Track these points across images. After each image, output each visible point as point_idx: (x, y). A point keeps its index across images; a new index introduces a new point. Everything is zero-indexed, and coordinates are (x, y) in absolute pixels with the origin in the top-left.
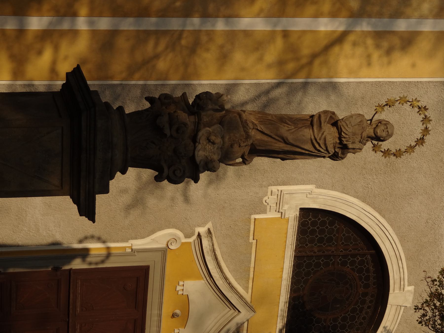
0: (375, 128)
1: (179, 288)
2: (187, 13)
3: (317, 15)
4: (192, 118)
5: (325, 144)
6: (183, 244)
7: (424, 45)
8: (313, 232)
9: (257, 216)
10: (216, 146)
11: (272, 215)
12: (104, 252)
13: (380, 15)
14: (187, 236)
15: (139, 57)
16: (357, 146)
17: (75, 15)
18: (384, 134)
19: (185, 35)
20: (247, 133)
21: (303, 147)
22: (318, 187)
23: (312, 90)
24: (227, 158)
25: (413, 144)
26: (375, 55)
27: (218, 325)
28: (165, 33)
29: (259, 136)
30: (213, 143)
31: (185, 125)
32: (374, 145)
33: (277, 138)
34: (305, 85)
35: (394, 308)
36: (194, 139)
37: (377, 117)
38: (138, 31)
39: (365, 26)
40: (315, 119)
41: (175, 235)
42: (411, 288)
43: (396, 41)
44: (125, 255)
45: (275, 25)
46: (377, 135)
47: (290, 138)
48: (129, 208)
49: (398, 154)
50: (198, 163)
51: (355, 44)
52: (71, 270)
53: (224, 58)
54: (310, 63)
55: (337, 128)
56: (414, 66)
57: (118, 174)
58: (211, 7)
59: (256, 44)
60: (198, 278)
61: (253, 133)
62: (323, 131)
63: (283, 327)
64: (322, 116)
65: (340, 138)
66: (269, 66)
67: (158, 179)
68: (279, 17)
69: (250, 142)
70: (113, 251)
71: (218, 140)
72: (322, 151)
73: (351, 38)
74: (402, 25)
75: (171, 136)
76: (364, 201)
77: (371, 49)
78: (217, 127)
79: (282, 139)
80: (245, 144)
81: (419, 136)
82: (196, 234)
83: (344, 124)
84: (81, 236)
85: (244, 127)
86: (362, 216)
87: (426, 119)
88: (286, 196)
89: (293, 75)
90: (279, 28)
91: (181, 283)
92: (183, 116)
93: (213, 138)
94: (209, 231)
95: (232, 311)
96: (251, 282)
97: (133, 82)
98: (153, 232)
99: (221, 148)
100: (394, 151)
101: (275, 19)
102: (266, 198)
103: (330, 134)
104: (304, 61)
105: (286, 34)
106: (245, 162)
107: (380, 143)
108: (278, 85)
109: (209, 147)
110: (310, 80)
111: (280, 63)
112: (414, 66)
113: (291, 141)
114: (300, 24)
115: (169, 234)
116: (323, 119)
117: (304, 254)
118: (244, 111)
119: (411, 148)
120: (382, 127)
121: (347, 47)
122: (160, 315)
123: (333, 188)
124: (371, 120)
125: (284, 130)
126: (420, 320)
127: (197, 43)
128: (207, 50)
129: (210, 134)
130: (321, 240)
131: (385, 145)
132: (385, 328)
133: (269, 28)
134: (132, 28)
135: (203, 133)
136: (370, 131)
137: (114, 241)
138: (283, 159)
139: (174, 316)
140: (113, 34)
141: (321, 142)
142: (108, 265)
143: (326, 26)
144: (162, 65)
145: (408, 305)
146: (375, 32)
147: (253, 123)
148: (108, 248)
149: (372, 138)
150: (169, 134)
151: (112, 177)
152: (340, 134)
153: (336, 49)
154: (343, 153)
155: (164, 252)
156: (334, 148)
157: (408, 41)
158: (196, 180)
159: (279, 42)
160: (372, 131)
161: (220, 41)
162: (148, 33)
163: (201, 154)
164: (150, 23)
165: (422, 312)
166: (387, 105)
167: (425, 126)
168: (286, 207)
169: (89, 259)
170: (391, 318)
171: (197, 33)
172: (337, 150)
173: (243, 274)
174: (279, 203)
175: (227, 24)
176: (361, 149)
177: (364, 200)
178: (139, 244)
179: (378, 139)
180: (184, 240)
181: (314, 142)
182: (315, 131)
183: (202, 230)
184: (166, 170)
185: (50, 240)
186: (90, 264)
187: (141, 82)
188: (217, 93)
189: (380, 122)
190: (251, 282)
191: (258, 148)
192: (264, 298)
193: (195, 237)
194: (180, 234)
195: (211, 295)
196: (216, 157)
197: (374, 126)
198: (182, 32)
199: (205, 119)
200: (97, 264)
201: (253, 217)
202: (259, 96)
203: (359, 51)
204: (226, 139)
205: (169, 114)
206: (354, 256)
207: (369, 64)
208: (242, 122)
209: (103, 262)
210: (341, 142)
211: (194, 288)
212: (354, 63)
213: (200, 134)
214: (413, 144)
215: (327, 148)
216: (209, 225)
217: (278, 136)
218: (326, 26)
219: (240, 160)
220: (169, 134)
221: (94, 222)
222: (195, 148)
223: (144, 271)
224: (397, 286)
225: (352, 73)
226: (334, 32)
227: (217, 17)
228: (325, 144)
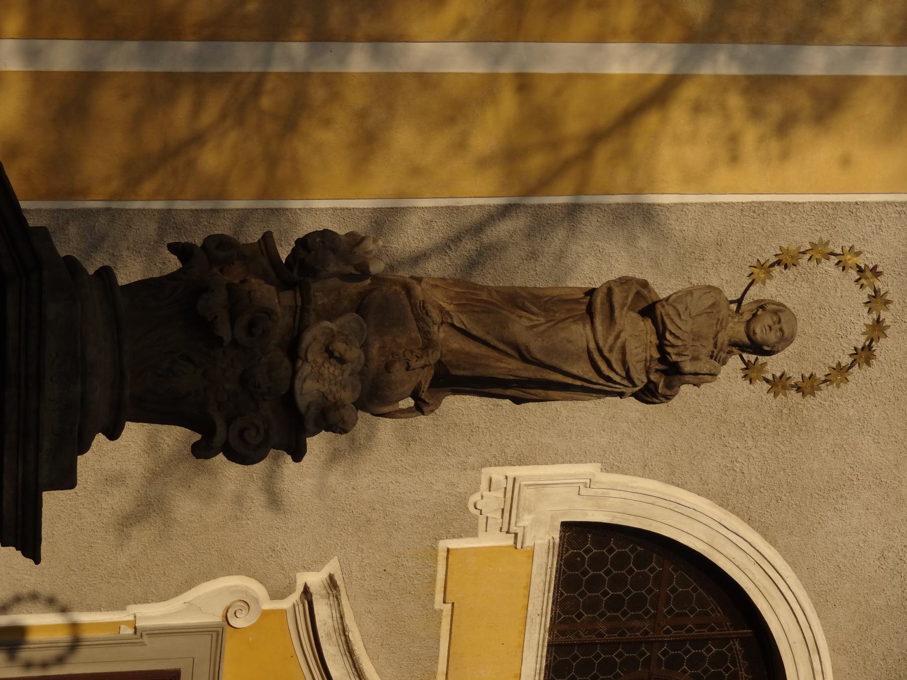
2: (274, 30)
3: (601, 37)
4: (288, 297)
5: (624, 363)
6: (265, 614)
7: (870, 109)
8: (595, 583)
9: (454, 544)
10: (348, 368)
11: (491, 539)
12: (64, 636)
13: (761, 36)
14: (276, 594)
15: (152, 141)
16: (704, 366)
18: (772, 337)
19: (269, 86)
20: (425, 334)
22: (609, 468)
23: (590, 224)
24: (374, 397)
25: (846, 360)
26: (750, 136)
28: (220, 78)
29: (458, 343)
30: (342, 361)
31: (270, 313)
33: (502, 347)
34: (573, 211)
36: (293, 350)
37: (755, 293)
38: (149, 75)
39: (722, 63)
40: (599, 300)
43: (802, 100)
45: (497, 60)
46: (756, 338)
47: (536, 347)
48: (126, 523)
49: (807, 386)
50: (303, 409)
51: (698, 108)
53: (368, 142)
54: (586, 155)
56: (846, 162)
57: (100, 438)
58: (336, 16)
59: (452, 106)
61: (440, 334)
65: (661, 348)
66: (483, 163)
67: (201, 451)
68: (508, 40)
69: (433, 357)
70: (87, 635)
71: (354, 353)
73: (689, 93)
74: (815, 61)
75: (235, 343)
76: (723, 503)
77: (739, 120)
78: (350, 319)
79: (511, 350)
81: (861, 341)
82: (300, 589)
83: (672, 312)
85: (418, 319)
86: (720, 542)
87: (877, 300)
88: (527, 493)
89: (543, 185)
90: (507, 69)
92: (265, 292)
93: (340, 347)
94: (332, 582)
97: (137, 205)
98: (189, 584)
99: (361, 373)
100: (796, 378)
102: (476, 497)
103: (637, 338)
104: (570, 150)
105: (524, 83)
106: (420, 408)
107: (762, 359)
108: (505, 211)
109: (331, 370)
110: (585, 199)
111: (511, 155)
112: (846, 162)
113: (539, 356)
116: (617, 298)
117: (572, 638)
118: (419, 280)
119: (840, 372)
120: (768, 320)
121: (678, 115)
123: (646, 471)
124: (739, 302)
125: (521, 327)
127: (299, 104)
128: (327, 122)
129: (332, 336)
130: (615, 604)
131: (774, 365)
133: (480, 68)
134: (134, 68)
135: (314, 336)
136: (736, 330)
137: (89, 609)
138: (518, 401)
140: (82, 87)
141: (614, 358)
143: (627, 62)
144: (211, 160)
146: (749, 77)
147: (441, 309)
148: (75, 626)
149: (742, 348)
150: (227, 338)
151: (84, 447)
152: (661, 336)
153: (651, 120)
155: (217, 634)
156: (648, 373)
157: (830, 100)
158: (298, 454)
159: (508, 104)
160: (742, 328)
161: (357, 98)
162: (174, 81)
164: (181, 55)
166: (778, 263)
168: (526, 520)
169: (24, 654)
171: (299, 81)
172: (653, 377)
174: (508, 511)
175: (376, 56)
176: (714, 375)
178: (152, 614)
179: (758, 348)
180: (269, 605)
181: (596, 356)
183: (315, 579)
184: (221, 429)
186: (28, 665)
187: (158, 205)
188: (351, 235)
189: (762, 305)
191: (454, 372)
193: (295, 597)
196: (347, 396)
197: (747, 316)
198: (261, 77)
199: (320, 300)
200: (45, 665)
201: (444, 544)
202: (456, 239)
203: (709, 124)
204: (375, 350)
205: (229, 287)
206: (699, 642)
207: (734, 159)
208: (413, 306)
209: (60, 661)
212: (695, 155)
213: (308, 337)
214: (846, 360)
215: (628, 371)
216: (332, 567)
217: (505, 343)
218: (627, 62)
219: (409, 402)
220: (227, 338)
222: (295, 372)
225: (692, 180)
226: (645, 77)
228: (624, 363)
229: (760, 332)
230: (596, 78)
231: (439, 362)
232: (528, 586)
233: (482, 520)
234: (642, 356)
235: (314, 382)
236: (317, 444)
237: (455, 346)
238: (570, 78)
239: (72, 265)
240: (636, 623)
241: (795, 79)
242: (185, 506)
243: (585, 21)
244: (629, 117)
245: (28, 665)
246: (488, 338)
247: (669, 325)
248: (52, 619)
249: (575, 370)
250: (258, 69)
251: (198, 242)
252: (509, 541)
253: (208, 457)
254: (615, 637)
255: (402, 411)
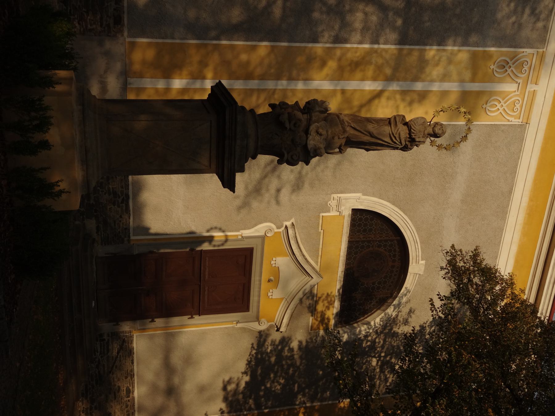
0: (433, 128)
1: (273, 262)
2: (278, 77)
3: (363, 79)
4: (305, 116)
5: (400, 138)
6: (275, 233)
9: (324, 214)
10: (322, 137)
12: (223, 239)
13: (405, 79)
14: (278, 228)
16: (422, 140)
17: (204, 78)
18: (440, 132)
20: (344, 129)
21: (384, 139)
22: (364, 195)
27: (298, 286)
29: (352, 132)
30: (321, 135)
31: (300, 120)
32: (431, 141)
33: (365, 133)
35: (412, 275)
36: (307, 132)
38: (246, 89)
39: (394, 87)
40: (392, 120)
41: (270, 227)
42: (423, 262)
43: (415, 96)
44: (238, 240)
46: (435, 134)
47: (375, 132)
48: (240, 208)
50: (309, 149)
51: (388, 98)
52: (202, 250)
55: (408, 127)
58: (294, 73)
60: (285, 255)
61: (348, 129)
62: (398, 128)
63: (340, 288)
64: (397, 117)
65: (410, 134)
67: (280, 162)
68: (339, 80)
69: (346, 135)
70: (230, 238)
71: (324, 133)
72: (397, 142)
73: (386, 94)
74: (419, 86)
75: (290, 129)
76: (393, 204)
77: (399, 102)
78: (323, 123)
80: (343, 137)
81: (464, 135)
82: (284, 226)
83: (413, 123)
84: (208, 227)
85: (342, 124)
86: (392, 214)
88: (343, 201)
90: (339, 88)
91: (274, 259)
92: (299, 114)
93: (320, 130)
95: (308, 277)
96: (320, 258)
98: (256, 225)
99: (326, 139)
101: (336, 82)
102: (330, 202)
105: (343, 92)
107: (436, 139)
109: (318, 138)
113: (376, 135)
114: (352, 85)
115: (267, 226)
117: (353, 240)
118: (341, 114)
120: (439, 127)
121: (383, 100)
122: (260, 281)
123: (374, 195)
124: (430, 122)
125: (371, 127)
126: (444, 276)
129: (318, 128)
131: (439, 141)
132: (406, 288)
133: (331, 88)
134: (241, 87)
135: (313, 128)
136: (430, 130)
137: (230, 232)
138: (367, 150)
139: (269, 281)
141: (397, 136)
142: (226, 247)
143: (370, 86)
145: (421, 274)
146: (402, 90)
147: (348, 122)
148: (226, 236)
149: (431, 135)
150: (288, 128)
152: (410, 131)
153: (376, 101)
154: (411, 145)
155: (263, 238)
156: (405, 141)
158: (307, 163)
159: (339, 97)
160: (431, 130)
162: (252, 91)
163: (311, 143)
164: (254, 84)
165: (446, 271)
166: (442, 111)
167: (468, 127)
168: (343, 208)
169: (213, 243)
170: (410, 281)
172: (407, 143)
173: (315, 253)
174: (338, 206)
176: (424, 142)
177: (393, 204)
178: (247, 233)
179: (436, 135)
180: (276, 230)
181: (392, 136)
182: (393, 127)
184: (286, 155)
185: (187, 230)
186: (214, 246)
188: (321, 101)
189: (436, 124)
190: (320, 258)
191: (352, 140)
192: (328, 268)
193: (283, 228)
194: (273, 226)
195: (293, 266)
196: (322, 146)
197: (432, 126)
198: (275, 90)
199: (314, 118)
200: (219, 246)
203: (391, 103)
204: (329, 133)
205: (288, 113)
208: (340, 121)
209: (223, 245)
210: (410, 137)
211: (282, 262)
213: (311, 128)
215: (400, 140)
216: (293, 220)
217: (366, 132)
218: (370, 86)
219: (337, 150)
220: (288, 128)
221: (234, 192)
222: (307, 138)
223: (250, 251)
224: (414, 261)
227: (298, 80)
228: (400, 138)
229: (437, 130)
230: (363, 91)
231: (347, 137)
232: (343, 226)
233: (331, 208)
234: (404, 136)
235: (313, 141)
236: (314, 160)
237: (352, 133)
238: (355, 91)
239: (243, 108)
240: (370, 236)
241: (414, 91)
242: (255, 204)
243: (359, 75)
244: (370, 101)
245: (214, 246)
246: (361, 130)
247: (412, 127)
248: (221, 234)
249: (386, 140)
250: (274, 88)
251: (278, 103)
252: (338, 214)
253: (281, 164)
254: (365, 239)
255: (336, 152)
